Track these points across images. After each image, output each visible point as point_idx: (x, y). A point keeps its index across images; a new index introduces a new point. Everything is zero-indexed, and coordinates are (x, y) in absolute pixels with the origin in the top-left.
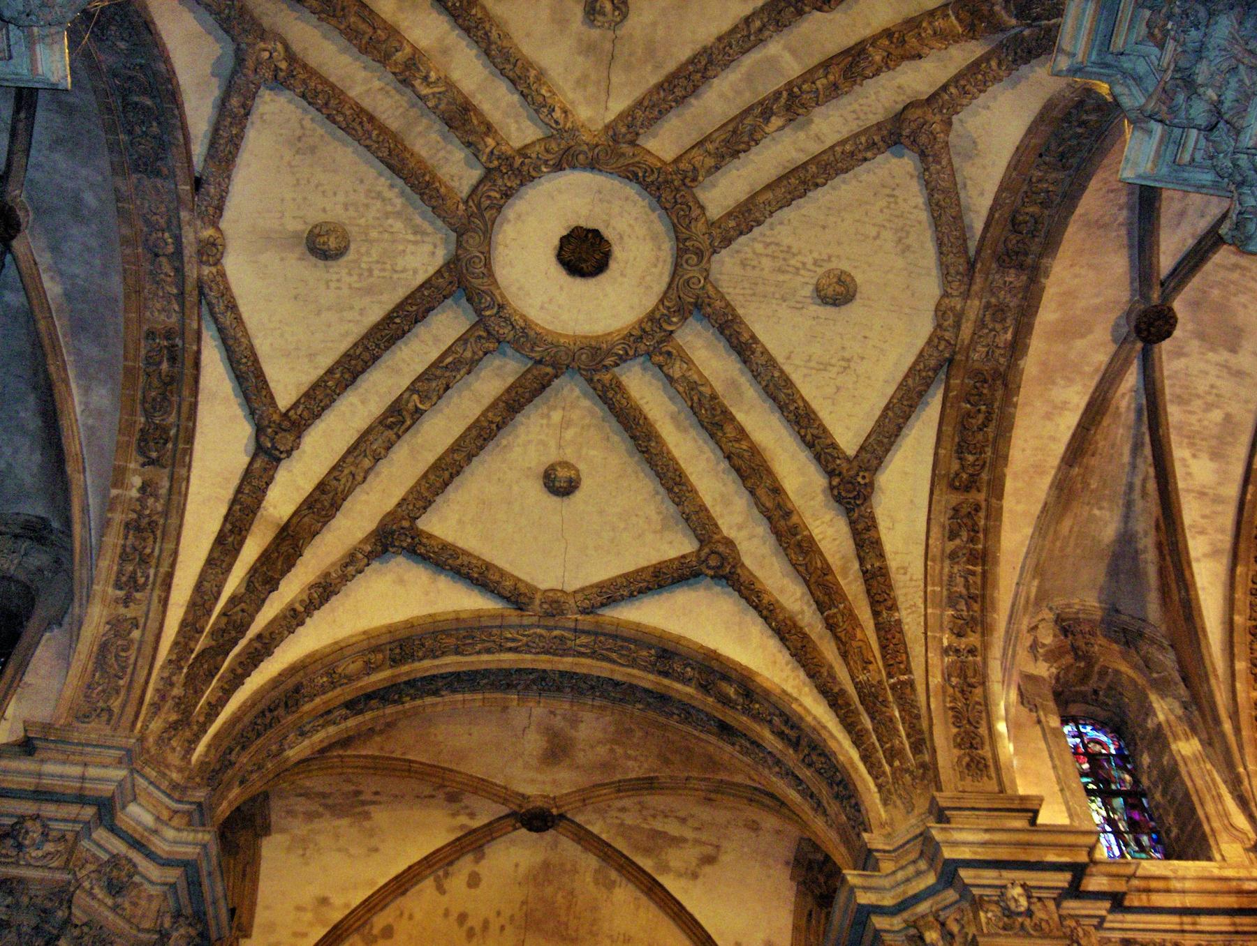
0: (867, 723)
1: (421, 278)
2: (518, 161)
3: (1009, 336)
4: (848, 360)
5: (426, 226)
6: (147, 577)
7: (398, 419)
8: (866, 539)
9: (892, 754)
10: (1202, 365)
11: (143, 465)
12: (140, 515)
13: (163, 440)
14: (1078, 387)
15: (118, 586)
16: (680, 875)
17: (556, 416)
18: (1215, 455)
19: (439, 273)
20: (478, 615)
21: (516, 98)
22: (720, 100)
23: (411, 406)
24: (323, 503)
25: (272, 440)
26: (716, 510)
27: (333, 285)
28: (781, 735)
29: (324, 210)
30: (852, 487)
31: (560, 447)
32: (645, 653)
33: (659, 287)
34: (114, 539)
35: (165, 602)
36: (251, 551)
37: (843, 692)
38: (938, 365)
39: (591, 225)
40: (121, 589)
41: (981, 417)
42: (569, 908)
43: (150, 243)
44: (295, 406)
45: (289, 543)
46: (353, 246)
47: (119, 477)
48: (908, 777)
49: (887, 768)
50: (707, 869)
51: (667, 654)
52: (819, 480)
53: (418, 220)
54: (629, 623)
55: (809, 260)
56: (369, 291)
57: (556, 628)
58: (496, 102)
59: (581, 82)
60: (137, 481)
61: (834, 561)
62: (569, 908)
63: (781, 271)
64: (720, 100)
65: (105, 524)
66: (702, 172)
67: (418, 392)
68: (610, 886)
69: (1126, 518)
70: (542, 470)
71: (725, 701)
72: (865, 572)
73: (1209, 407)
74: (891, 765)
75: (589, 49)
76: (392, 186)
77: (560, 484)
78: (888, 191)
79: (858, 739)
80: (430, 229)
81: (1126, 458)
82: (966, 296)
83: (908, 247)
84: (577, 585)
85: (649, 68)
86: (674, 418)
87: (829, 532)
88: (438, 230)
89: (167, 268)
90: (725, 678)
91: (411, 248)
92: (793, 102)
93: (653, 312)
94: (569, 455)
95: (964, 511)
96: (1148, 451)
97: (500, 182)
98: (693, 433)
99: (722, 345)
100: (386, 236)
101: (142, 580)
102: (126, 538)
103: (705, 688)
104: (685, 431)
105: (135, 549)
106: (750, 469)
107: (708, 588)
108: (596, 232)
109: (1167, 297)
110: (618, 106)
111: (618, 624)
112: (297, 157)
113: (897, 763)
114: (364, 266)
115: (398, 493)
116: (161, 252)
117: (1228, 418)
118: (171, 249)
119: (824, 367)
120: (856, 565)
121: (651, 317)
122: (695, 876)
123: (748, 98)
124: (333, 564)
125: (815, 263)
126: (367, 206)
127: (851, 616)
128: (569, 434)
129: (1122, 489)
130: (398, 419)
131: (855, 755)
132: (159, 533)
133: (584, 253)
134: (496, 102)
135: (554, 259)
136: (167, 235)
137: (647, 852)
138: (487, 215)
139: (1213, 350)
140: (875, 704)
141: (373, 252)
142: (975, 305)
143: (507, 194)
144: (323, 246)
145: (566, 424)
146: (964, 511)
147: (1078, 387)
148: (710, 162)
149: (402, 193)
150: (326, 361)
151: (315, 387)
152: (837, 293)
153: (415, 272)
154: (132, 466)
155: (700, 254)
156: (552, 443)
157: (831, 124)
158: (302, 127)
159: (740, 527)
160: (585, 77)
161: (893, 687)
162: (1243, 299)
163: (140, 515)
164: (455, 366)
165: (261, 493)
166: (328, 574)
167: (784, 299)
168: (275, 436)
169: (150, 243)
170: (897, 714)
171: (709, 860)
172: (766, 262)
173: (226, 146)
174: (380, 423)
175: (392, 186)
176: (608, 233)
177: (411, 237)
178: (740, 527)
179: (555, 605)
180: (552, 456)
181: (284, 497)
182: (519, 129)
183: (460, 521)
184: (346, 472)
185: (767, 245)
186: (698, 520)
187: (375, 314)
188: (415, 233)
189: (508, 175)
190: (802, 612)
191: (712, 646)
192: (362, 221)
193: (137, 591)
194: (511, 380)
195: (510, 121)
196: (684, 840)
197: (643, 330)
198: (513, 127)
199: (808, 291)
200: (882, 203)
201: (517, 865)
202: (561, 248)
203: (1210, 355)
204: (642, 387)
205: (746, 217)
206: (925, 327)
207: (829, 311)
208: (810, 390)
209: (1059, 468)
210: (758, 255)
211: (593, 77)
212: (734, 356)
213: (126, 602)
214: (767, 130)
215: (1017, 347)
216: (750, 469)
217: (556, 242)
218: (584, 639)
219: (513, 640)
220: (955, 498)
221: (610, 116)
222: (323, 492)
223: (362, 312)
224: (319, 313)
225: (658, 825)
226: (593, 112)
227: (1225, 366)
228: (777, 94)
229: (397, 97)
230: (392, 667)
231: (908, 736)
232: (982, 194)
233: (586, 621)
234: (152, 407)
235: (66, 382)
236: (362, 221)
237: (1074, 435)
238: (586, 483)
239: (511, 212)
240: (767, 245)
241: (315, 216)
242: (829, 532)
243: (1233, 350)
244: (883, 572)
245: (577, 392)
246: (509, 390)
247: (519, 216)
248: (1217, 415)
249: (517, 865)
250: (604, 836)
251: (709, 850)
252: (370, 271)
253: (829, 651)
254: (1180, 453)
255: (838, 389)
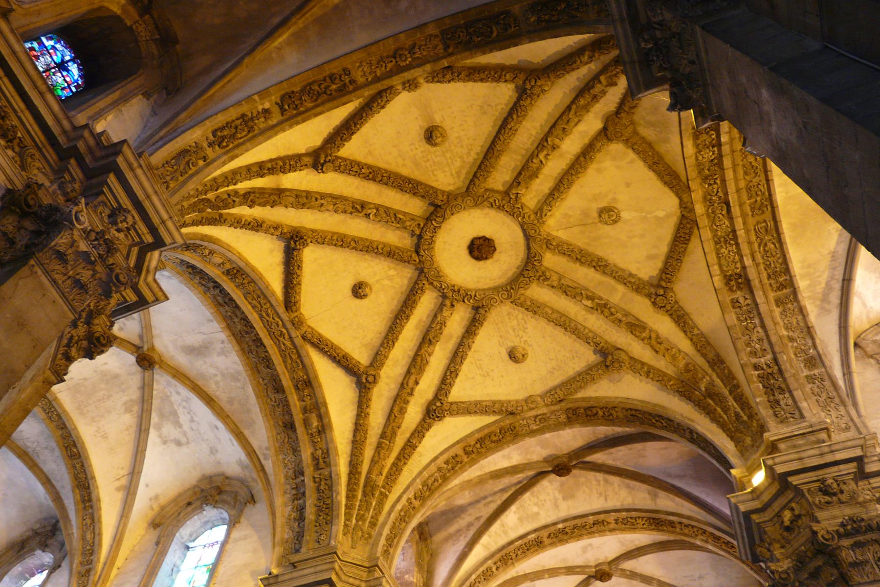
0: (360, 495)
1: (434, 184)
2: (519, 206)
3: (535, 428)
4: (488, 375)
5: (463, 176)
6: (227, 146)
7: (359, 208)
8: (420, 432)
9: (360, 518)
10: (550, 492)
11: (277, 103)
12: (252, 119)
13: (295, 105)
14: (519, 458)
15: (214, 133)
16: (160, 437)
17: (392, 272)
18: (521, 519)
19: (443, 192)
20: (273, 294)
21: (547, 191)
22: (584, 275)
23: (369, 211)
24: (304, 199)
25: (325, 161)
26: (389, 362)
27: (413, 147)
28: (315, 459)
29: (452, 128)
30: (434, 412)
31: (377, 281)
32: (301, 374)
33: (481, 286)
34: (233, 114)
35: (224, 163)
36: (259, 183)
37: (360, 473)
38: (508, 410)
39: (497, 246)
40: (214, 136)
41: (496, 438)
42: (99, 400)
43: (401, 52)
44: (345, 159)
45: (276, 197)
46: (437, 148)
47: (263, 94)
48: (360, 533)
49: (354, 521)
50: (173, 446)
51: (308, 384)
52: (430, 395)
53: (464, 172)
54: (310, 358)
55: (525, 338)
56: (417, 164)
57: (286, 329)
58: (542, 185)
59: (566, 216)
60: (267, 105)
61: (404, 426)
62: (99, 400)
63: (514, 330)
64: (584, 275)
65: (238, 103)
66: (549, 282)
67: (377, 210)
68: (128, 410)
69: (471, 504)
70: (361, 279)
71: (306, 423)
72: (409, 441)
73: (536, 504)
74: (357, 521)
75: (585, 214)
76: (478, 154)
77: (359, 291)
78: (575, 355)
79: (350, 497)
80: (462, 179)
81: (496, 489)
82: (547, 405)
83: (553, 373)
84: (312, 325)
85: (586, 241)
86: (420, 320)
87: (413, 413)
88: (463, 182)
89: (390, 66)
90: (320, 417)
91: (448, 174)
92: (602, 308)
93: (469, 290)
94: (374, 288)
95: (458, 459)
96: (506, 496)
97: (504, 202)
98: (418, 332)
99: (465, 323)
100: (450, 161)
101: (225, 144)
102: (237, 119)
103: (305, 410)
104: (417, 329)
105: (236, 128)
106: (417, 364)
107: (351, 381)
108: (495, 250)
109: (574, 466)
110: (562, 235)
111: (308, 355)
112: (478, 108)
113: (360, 523)
114: (429, 157)
115: (318, 226)
116: (398, 59)
117: (537, 514)
118: (403, 64)
119: (480, 367)
120: (408, 435)
121: (466, 291)
122: (165, 443)
123: (591, 286)
124: (269, 220)
125: (525, 341)
126: (462, 146)
127: (390, 449)
128: (386, 282)
129: (482, 495)
130: (359, 208)
131: (344, 501)
132: (251, 135)
133: (480, 249)
134: (542, 185)
135: (472, 237)
136: (410, 59)
137: (162, 415)
138: (485, 203)
139: (559, 492)
140: (368, 490)
141: (438, 158)
142: (545, 410)
143: (500, 208)
144: (431, 135)
145: (390, 278)
146: (458, 459)
147: (519, 458)
148: (555, 284)
149: (475, 160)
150: (370, 161)
151: (358, 164)
152: (514, 356)
153: (436, 181)
154: (273, 98)
155: (509, 297)
156: (377, 278)
157: (595, 323)
158: (497, 105)
159: (388, 377)
160: (570, 216)
161: (381, 493)
162: (587, 490)
163: (252, 119)
164: (399, 221)
165: (293, 169)
166: (264, 222)
167: (501, 337)
168: (319, 159)
169: (401, 52)
170: (374, 504)
171: (179, 443)
172: (515, 323)
173: (477, 74)
174: (353, 202)
175: (478, 154)
176: (496, 255)
177: (454, 172)
178: (388, 377)
179: (298, 323)
180: (370, 280)
181: (292, 180)
182: (531, 199)
183: (316, 260)
184: (322, 201)
185: (523, 319)
186: (378, 358)
187: (405, 172)
188: (457, 173)
189: (507, 202)
190: (373, 428)
191: (328, 401)
192: (453, 147)
193: (219, 146)
194: (400, 245)
195: (534, 193)
196: (180, 426)
197: (459, 291)
198: (531, 196)
199: (511, 344)
200: (568, 355)
201: (106, 364)
202: (479, 238)
203: (556, 492)
204: (427, 302)
205: (534, 308)
206: (521, 396)
207: (507, 357)
208: (466, 368)
209: (486, 474)
210: (516, 318)
211: (571, 220)
212: (463, 330)
213: (210, 145)
214: (583, 301)
215: (532, 433)
216: (417, 364)
217: (481, 234)
218: (288, 344)
219: (268, 315)
220: (461, 453)
221: (555, 233)
222: (307, 198)
223: (404, 165)
224: (394, 146)
225: (180, 411)
226: (555, 224)
227: (556, 500)
228: (601, 299)
229: (529, 143)
230: (223, 273)
231: (372, 517)
232: (596, 391)
233: (299, 341)
234: (307, 89)
235: (289, 28)
236: (453, 147)
237: (500, 470)
238: (365, 302)
239: (492, 213)
240: (523, 319)
241: (447, 124)
242: (413, 413)
243: (564, 499)
244: (414, 448)
245: (409, 275)
246: (397, 248)
247: (487, 214)
248: (535, 509)
249: (106, 364)
250: (154, 393)
251: (184, 440)
252: (428, 160)
253: (368, 453)
254: (513, 508)
255: (473, 378)
